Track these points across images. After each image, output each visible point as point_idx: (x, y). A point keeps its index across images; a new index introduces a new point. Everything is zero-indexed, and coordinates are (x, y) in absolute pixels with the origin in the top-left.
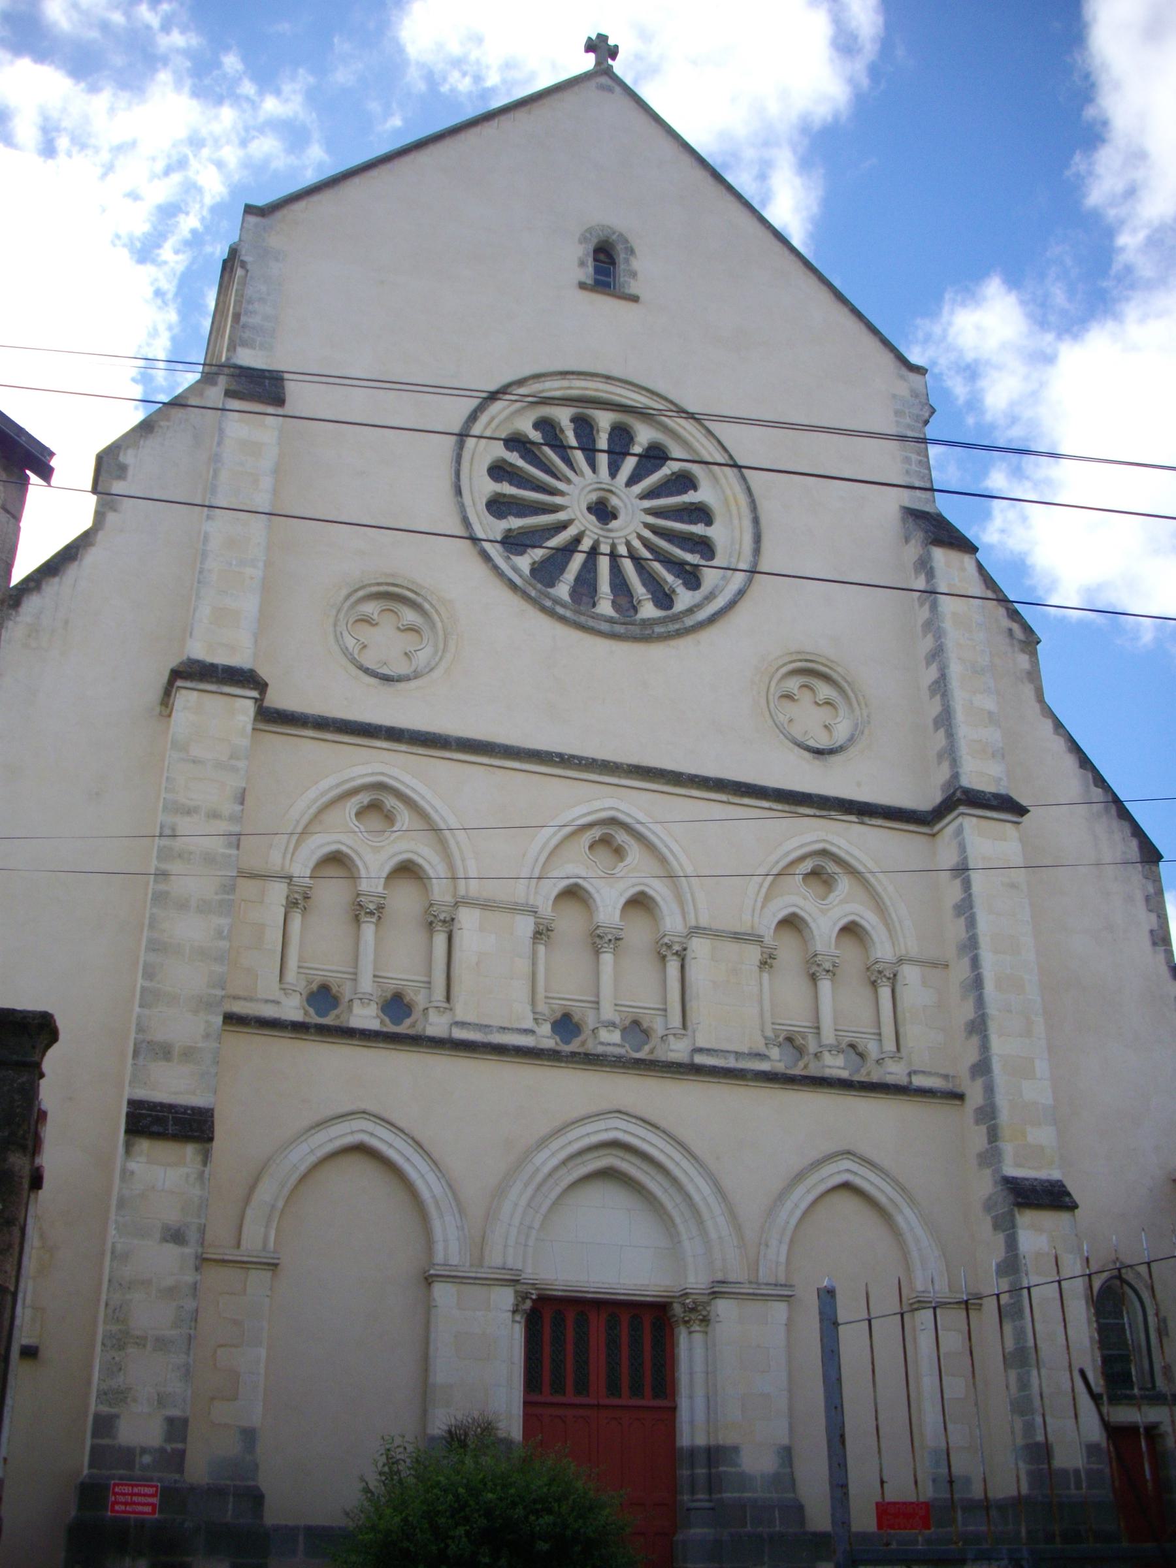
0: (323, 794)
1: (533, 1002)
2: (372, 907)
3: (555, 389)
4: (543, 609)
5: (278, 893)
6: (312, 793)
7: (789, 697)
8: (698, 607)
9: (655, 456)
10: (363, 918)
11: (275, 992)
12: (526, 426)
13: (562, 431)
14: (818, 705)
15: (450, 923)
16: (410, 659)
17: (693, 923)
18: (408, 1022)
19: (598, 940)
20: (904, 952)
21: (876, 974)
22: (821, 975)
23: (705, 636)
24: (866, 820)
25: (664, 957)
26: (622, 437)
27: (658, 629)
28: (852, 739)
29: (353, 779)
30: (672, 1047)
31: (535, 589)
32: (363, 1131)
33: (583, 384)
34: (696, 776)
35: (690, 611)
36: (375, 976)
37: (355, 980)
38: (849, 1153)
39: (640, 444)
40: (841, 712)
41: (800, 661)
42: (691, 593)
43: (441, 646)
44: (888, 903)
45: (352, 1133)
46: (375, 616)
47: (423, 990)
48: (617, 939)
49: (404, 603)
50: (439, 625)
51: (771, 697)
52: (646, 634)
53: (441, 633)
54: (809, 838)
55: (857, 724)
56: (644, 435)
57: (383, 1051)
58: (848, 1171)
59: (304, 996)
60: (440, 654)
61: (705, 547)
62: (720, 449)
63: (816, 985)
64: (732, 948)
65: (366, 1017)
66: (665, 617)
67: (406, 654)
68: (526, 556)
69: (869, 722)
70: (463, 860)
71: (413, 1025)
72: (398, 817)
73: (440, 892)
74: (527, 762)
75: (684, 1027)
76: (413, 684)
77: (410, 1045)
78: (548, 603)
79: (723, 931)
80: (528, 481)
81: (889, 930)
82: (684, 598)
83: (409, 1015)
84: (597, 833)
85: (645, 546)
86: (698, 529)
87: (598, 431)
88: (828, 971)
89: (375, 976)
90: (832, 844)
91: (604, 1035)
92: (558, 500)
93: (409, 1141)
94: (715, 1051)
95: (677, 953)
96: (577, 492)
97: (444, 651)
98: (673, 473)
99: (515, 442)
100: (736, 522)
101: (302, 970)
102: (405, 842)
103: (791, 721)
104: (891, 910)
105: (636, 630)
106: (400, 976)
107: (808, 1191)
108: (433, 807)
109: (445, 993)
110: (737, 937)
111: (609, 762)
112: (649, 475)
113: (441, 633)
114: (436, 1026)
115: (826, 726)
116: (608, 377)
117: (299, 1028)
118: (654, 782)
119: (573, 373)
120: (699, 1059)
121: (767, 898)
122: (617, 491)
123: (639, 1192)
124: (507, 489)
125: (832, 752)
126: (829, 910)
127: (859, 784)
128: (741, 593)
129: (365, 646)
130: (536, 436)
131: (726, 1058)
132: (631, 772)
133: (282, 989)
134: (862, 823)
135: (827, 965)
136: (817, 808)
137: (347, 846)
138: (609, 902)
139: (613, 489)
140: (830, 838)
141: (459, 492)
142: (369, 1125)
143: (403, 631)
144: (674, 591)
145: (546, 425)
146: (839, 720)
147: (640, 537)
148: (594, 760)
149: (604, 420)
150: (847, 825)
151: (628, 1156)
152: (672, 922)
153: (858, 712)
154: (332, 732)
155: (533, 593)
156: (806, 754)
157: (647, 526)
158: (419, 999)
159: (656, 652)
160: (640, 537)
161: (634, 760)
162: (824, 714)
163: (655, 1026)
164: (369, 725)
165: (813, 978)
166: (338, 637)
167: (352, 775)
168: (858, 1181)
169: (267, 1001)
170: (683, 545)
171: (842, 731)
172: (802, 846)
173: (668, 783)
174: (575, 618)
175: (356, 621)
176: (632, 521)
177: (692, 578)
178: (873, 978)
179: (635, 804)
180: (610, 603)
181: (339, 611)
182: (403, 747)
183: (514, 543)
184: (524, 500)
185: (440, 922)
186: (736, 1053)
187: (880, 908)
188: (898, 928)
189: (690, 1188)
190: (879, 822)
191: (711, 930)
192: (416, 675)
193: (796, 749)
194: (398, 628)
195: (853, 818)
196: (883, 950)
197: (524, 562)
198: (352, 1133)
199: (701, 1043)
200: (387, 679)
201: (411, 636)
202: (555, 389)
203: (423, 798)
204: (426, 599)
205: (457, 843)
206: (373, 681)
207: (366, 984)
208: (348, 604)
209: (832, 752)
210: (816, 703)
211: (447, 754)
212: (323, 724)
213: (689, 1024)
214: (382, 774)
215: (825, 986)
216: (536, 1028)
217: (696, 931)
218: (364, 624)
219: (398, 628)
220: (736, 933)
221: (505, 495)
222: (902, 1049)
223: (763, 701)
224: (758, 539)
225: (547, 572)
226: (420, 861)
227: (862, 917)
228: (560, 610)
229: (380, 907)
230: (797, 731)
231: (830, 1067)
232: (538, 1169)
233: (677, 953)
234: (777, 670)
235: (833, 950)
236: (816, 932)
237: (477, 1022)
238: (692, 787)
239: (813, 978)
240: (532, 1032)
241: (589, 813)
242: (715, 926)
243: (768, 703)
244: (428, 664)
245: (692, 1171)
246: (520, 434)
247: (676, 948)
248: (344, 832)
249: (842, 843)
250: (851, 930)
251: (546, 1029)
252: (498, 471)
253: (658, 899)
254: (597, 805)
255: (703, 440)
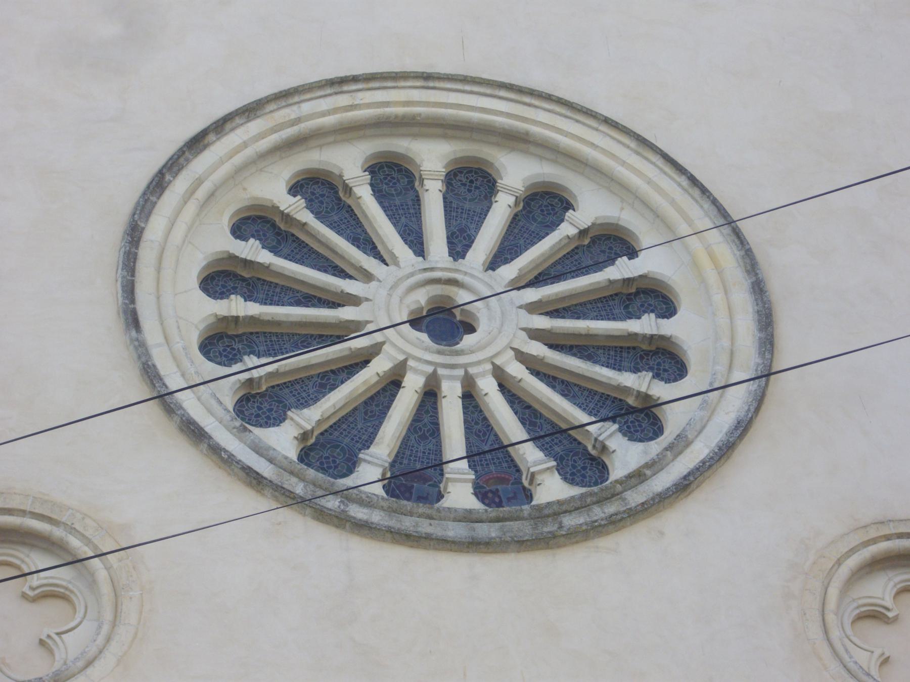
3: (324, 114)
4: (323, 516)
7: (874, 615)
8: (654, 466)
9: (544, 205)
12: (274, 189)
13: (348, 190)
16: (51, 652)
23: (674, 520)
26: (471, 185)
27: (571, 521)
31: (302, 479)
33: (379, 96)
35: (638, 477)
39: (509, 191)
41: (888, 538)
42: (640, 446)
43: (108, 615)
49: (33, 546)
51: (831, 618)
52: (548, 533)
53: (105, 588)
56: (516, 174)
60: (106, 629)
61: (666, 360)
62: (668, 169)
66: (582, 496)
67: (42, 643)
68: (287, 424)
78: (332, 503)
80: (286, 289)
82: (626, 456)
85: (536, 373)
86: (645, 325)
87: (422, 180)
92: (347, 313)
96: (383, 292)
97: (114, 624)
98: (583, 233)
99: (256, 222)
100: (718, 297)
105: (522, 528)
112: (533, 244)
113: (105, 588)
116: (427, 77)
119: (355, 79)
122: (467, 280)
124: (238, 306)
128: (742, 428)
130: (296, 207)
139: (459, 277)
141: (133, 320)
143: (34, 600)
144: (604, 448)
145: (319, 188)
147: (521, 357)
149: (432, 158)
155: (299, 489)
157: (535, 334)
159: (569, 566)
160: (521, 357)
170: (617, 353)
174: (393, 523)
176: (506, 327)
177: (642, 419)
180: (469, 488)
183: (259, 406)
184: (278, 323)
194: (24, 596)
197: (283, 439)
201: (52, 607)
202: (324, 114)
204: (72, 530)
219: (24, 596)
221: (236, 319)
223: (815, 631)
224: (766, 320)
225: (331, 451)
228: (357, 512)
234: (839, 563)
243: (826, 632)
244: (83, 653)
246: (262, 207)
252: (220, 279)
255: (634, 160)
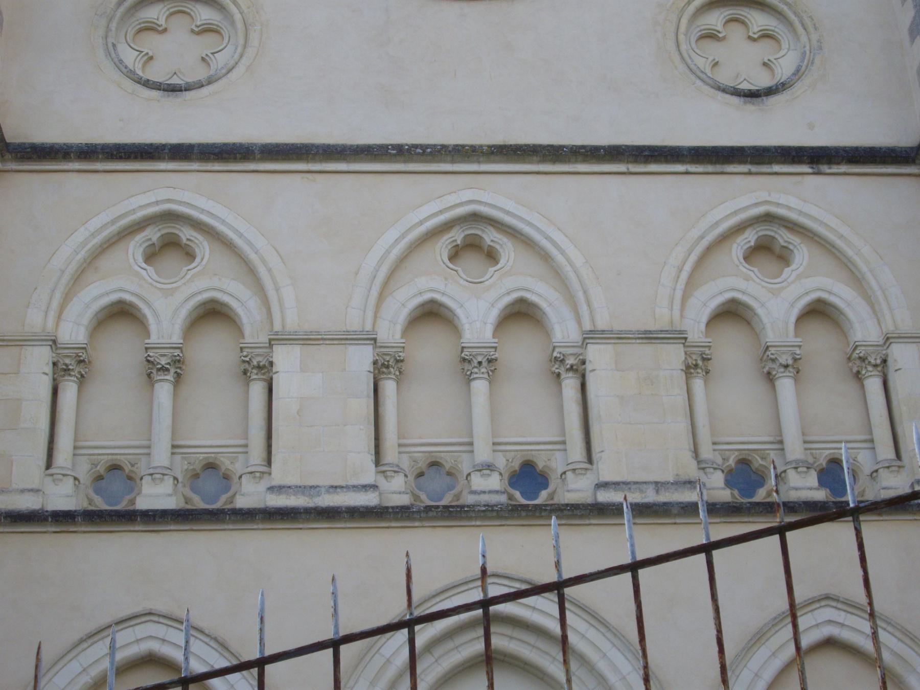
0: (93, 235)
1: (696, 452)
2: (163, 361)
5: (39, 360)
6: (80, 235)
7: (711, 36)
10: (157, 376)
11: (369, 476)
14: (754, 40)
15: (266, 369)
17: (588, 326)
18: (544, 494)
19: (467, 366)
20: (891, 328)
21: (858, 362)
22: (778, 372)
24: (825, 168)
25: (559, 375)
28: (798, 73)
29: (134, 211)
30: (572, 486)
32: (151, 637)
34: (583, 147)
36: (400, 445)
37: (783, 449)
38: (827, 597)
40: (785, 45)
44: (864, 269)
45: (138, 641)
46: (162, 21)
47: (558, 454)
48: (490, 361)
50: (238, 17)
53: (240, 25)
54: (744, 201)
55: (804, 54)
57: (420, 530)
58: (830, 622)
59: (506, 476)
60: (239, 50)
63: (862, 387)
64: (646, 351)
65: (156, 495)
69: (821, 48)
70: (277, 290)
71: (551, 496)
72: (197, 250)
73: (254, 330)
74: (355, 161)
75: (590, 460)
76: (205, 91)
77: (210, 521)
79: (630, 332)
81: (872, 305)
83: (545, 485)
84: (457, 235)
88: (786, 366)
89: (714, 443)
90: (778, 205)
91: (478, 482)
93: (212, 643)
94: (626, 483)
95: (571, 368)
97: (245, 47)
101: (403, 449)
102: (207, 277)
103: (716, 64)
104: (869, 276)
106: (209, 443)
107: (774, 654)
108: (236, 231)
109: (264, 455)
110: (649, 337)
111: (463, 146)
113: (240, 25)
114: (250, 495)
115: (765, 64)
117: (183, 517)
118: (524, 162)
120: (604, 497)
121: (691, 284)
123: (542, 679)
125: (770, 92)
126: (783, 288)
127: (811, 126)
129: (151, 58)
131: (641, 491)
132: (492, 153)
133: (699, 469)
134: (819, 173)
135: (785, 359)
136: (752, 163)
137: (132, 294)
138: (477, 316)
140: (774, 197)
142: (159, 630)
143: (198, 33)
146: (782, 53)
148: (444, 147)
150: (799, 178)
151: (517, 633)
152: (564, 330)
153: (804, 39)
154: (102, 161)
156: (735, 100)
158: (556, 464)
161: (499, 139)
162: (763, 50)
163: (553, 464)
164: (151, 145)
165: (770, 378)
166: (111, 50)
167: (131, 208)
168: (845, 635)
169: (23, 491)
171: (785, 67)
172: (735, 213)
173: (543, 160)
175: (140, 31)
178: (855, 370)
179: (500, 193)
181: (110, 20)
182: (195, 166)
185: (257, 370)
186: (656, 483)
187: (856, 279)
188: (881, 299)
189: (602, 666)
190: (843, 168)
191: (611, 332)
192: (210, 81)
193: (720, 95)
194: (192, 31)
195: (805, 168)
196: (865, 331)
198: (138, 641)
199: (606, 477)
200: (173, 89)
203: (223, 222)
205: (270, 270)
206: (155, 94)
207: (161, 456)
208: (122, 9)
209: (770, 92)
210: (750, 38)
211: (252, 166)
212: (88, 153)
213: (595, 456)
214: (169, 201)
215: (786, 385)
216: (704, 479)
217: (591, 336)
218: (151, 33)
219: (192, 31)
220: (646, 332)
222: (904, 455)
223: (671, 45)
226: (225, 299)
227: (830, 293)
229: (178, 362)
230: (725, 77)
231: (796, 489)
232: (388, 661)
233: (571, 368)
235: (791, 338)
236: (765, 320)
237: (299, 483)
238: (576, 162)
239: (770, 378)
240: (374, 487)
241: (441, 212)
242: (617, 327)
243: (678, 46)
245: (605, 646)
247: (570, 361)
248: (125, 275)
249: (793, 202)
250: (818, 312)
251: (717, 479)
253: (543, 305)
254: (452, 200)
